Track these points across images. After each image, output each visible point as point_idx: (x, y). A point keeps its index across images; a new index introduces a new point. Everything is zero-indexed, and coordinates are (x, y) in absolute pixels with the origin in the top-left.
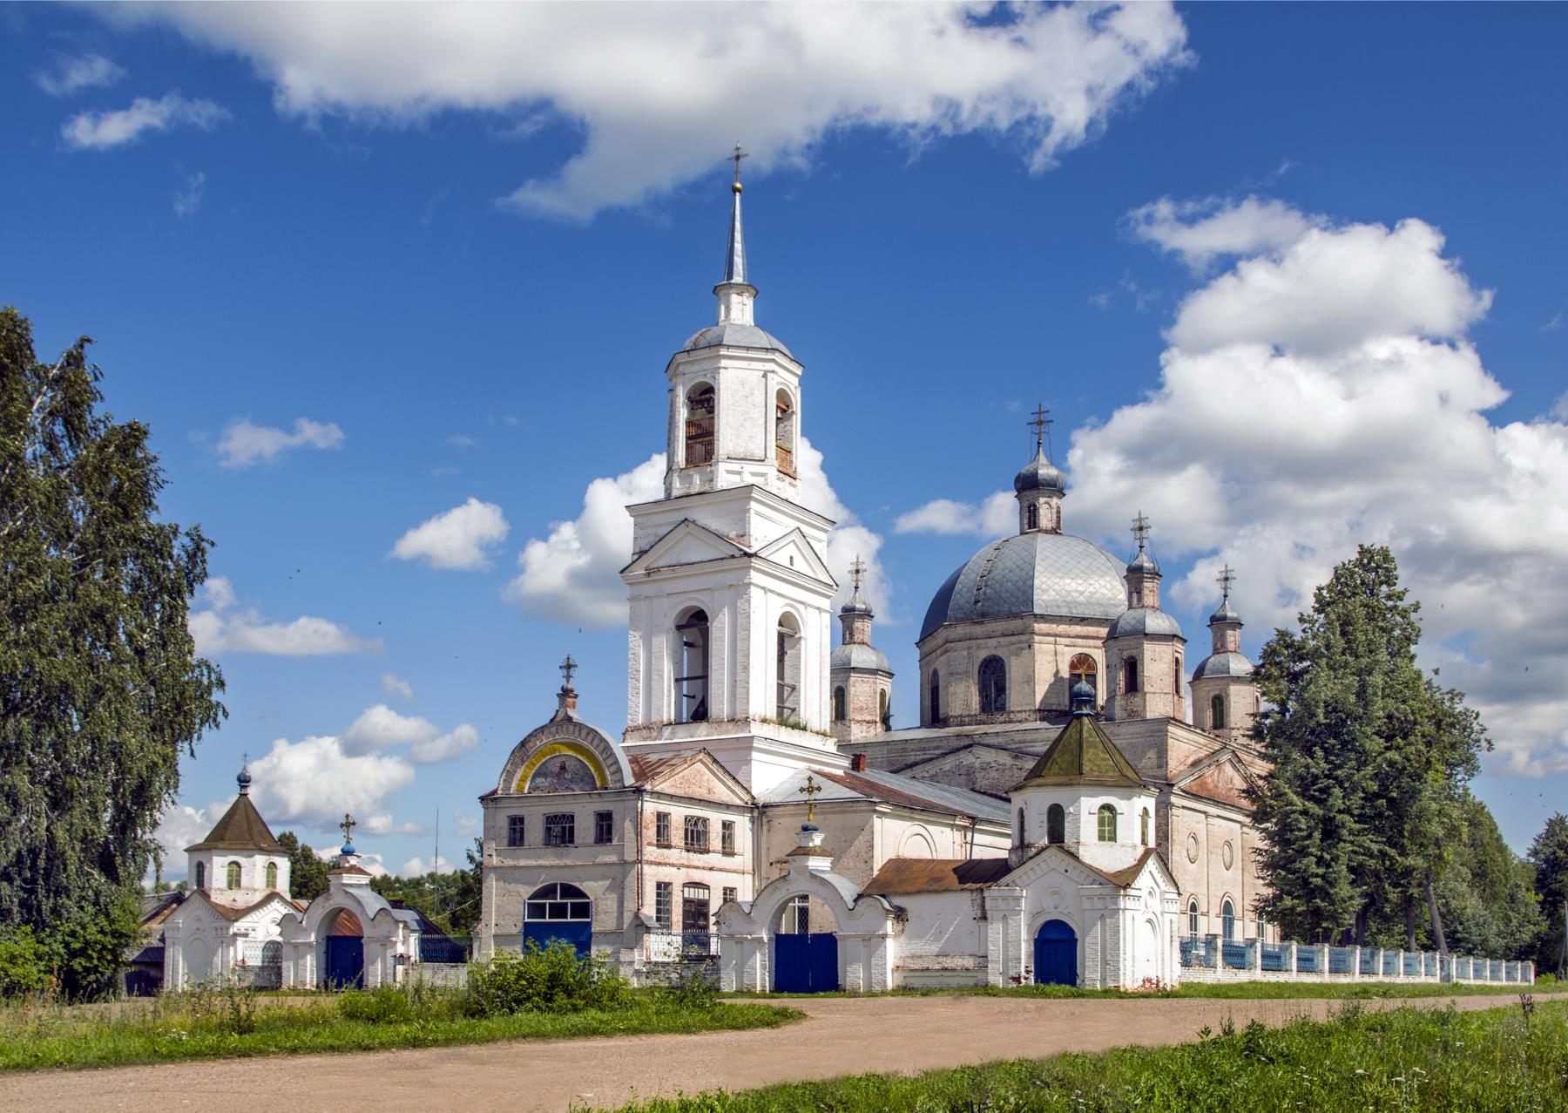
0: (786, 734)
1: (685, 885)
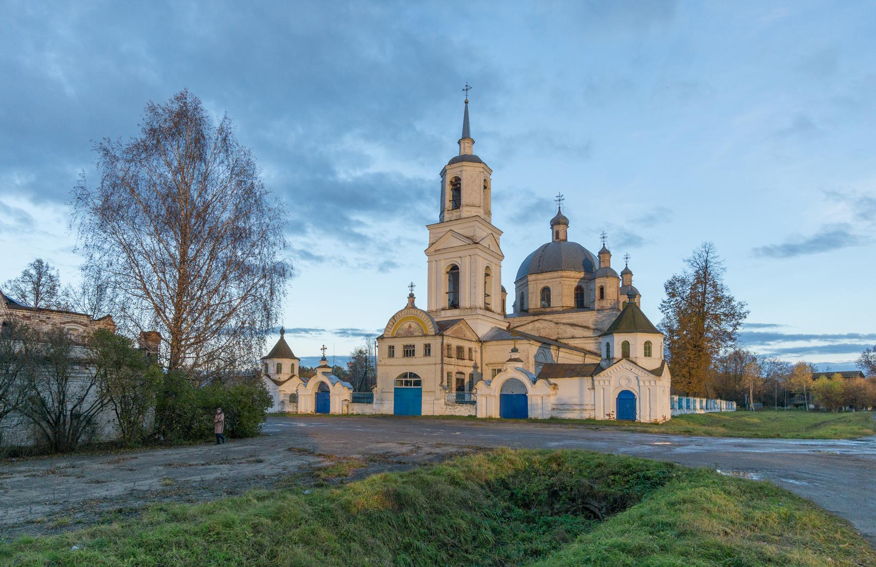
0: (488, 313)
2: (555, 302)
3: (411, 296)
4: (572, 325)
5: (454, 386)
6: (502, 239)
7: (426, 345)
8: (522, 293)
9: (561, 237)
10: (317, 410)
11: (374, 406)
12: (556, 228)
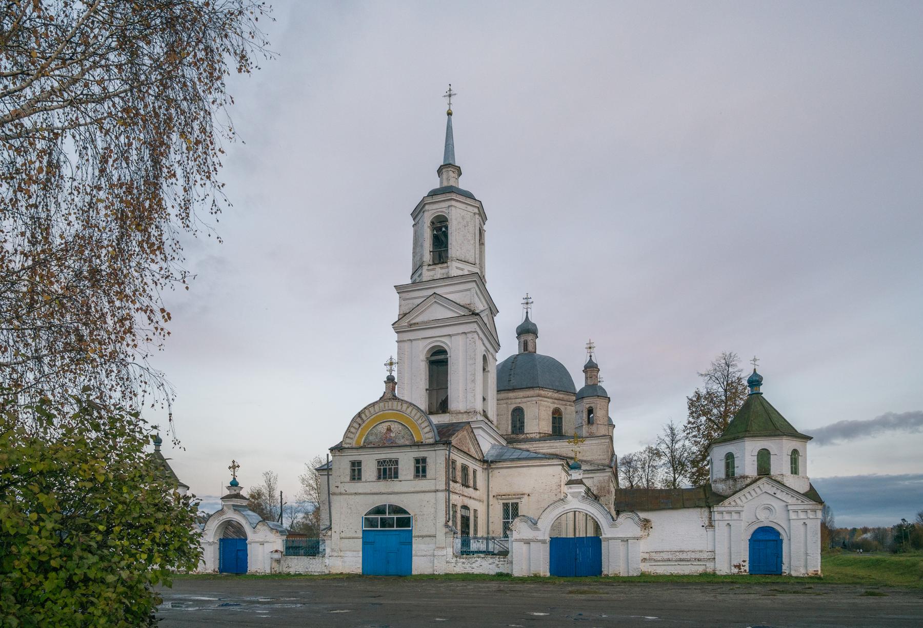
7: (417, 461)
9: (530, 348)
10: (221, 570)
11: (327, 561)
12: (523, 338)
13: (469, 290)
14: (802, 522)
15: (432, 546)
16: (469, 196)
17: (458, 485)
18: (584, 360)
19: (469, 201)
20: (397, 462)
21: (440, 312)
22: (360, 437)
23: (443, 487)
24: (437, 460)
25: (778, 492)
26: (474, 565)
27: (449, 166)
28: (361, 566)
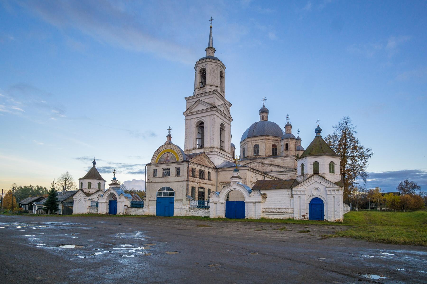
0: (222, 152)
1: (199, 188)
2: (262, 152)
3: (169, 136)
4: (271, 165)
5: (197, 196)
6: (232, 110)
8: (244, 148)
9: (265, 119)
13: (213, 97)
14: (333, 196)
15: (182, 204)
16: (217, 59)
17: (197, 178)
18: (285, 123)
19: (215, 61)
20: (170, 169)
21: (201, 107)
22: (157, 160)
23: (186, 179)
24: (184, 168)
25: (322, 181)
26: (196, 213)
27: (210, 48)
28: (155, 212)
